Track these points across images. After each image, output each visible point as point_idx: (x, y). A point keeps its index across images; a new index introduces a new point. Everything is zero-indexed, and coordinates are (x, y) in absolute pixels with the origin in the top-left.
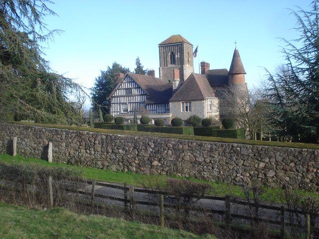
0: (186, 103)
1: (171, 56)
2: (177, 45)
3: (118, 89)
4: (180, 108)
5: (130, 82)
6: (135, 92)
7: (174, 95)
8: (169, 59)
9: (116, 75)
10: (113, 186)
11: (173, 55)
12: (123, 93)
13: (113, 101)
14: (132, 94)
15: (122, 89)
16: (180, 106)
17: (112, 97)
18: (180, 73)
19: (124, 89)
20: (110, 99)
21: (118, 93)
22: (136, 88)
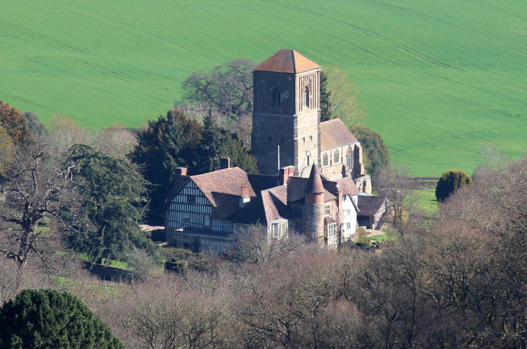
15: (183, 195)
19: (186, 195)
21: (178, 199)
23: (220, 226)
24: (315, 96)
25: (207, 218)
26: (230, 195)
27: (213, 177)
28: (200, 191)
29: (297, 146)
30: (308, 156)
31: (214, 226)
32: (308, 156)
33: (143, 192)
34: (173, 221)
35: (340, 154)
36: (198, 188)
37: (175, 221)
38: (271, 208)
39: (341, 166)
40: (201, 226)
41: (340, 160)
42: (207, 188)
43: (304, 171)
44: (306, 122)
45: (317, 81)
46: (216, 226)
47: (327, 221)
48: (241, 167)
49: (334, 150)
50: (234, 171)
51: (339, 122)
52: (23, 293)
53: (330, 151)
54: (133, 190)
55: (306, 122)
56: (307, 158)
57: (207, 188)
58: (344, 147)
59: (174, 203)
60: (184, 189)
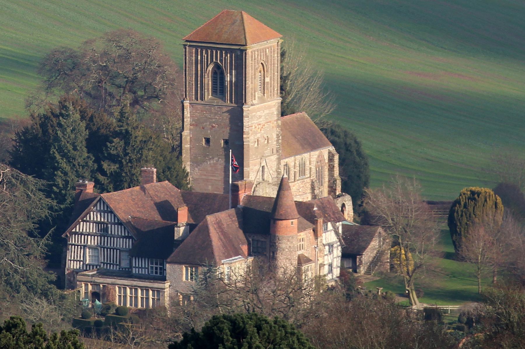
0: (192, 268)
1: (214, 73)
2: (231, 51)
3: (83, 221)
4: (182, 275)
5: (104, 212)
6: (114, 230)
7: (176, 251)
8: (208, 81)
9: (80, 186)
10: (186, 58)
11: (218, 74)
12: (92, 228)
13: (73, 240)
14: (107, 232)
15: (89, 222)
16: (182, 271)
17: (72, 234)
18: (231, 121)
19: (94, 222)
20: (67, 236)
21: (82, 227)
22: (115, 224)
23: (145, 268)
24: (273, 80)
25: (125, 256)
26: (218, 211)
27: (132, 195)
28: (115, 216)
29: (248, 151)
30: (263, 167)
31: (135, 267)
32: (263, 167)
33: (43, 216)
34: (74, 261)
35: (308, 163)
36: (112, 212)
37: (77, 261)
38: (221, 240)
39: (309, 180)
40: (116, 268)
41: (307, 172)
42: (125, 212)
43: (257, 189)
44: (260, 117)
45: (276, 56)
46: (139, 268)
47: (302, 261)
48: (169, 180)
49: (298, 157)
50: (163, 187)
51: (303, 118)
52: (215, 321)
53: (293, 158)
54: (358, 154)
55: (260, 117)
56: (261, 169)
57: (125, 212)
58: (312, 153)
59: (76, 233)
60: (92, 213)
